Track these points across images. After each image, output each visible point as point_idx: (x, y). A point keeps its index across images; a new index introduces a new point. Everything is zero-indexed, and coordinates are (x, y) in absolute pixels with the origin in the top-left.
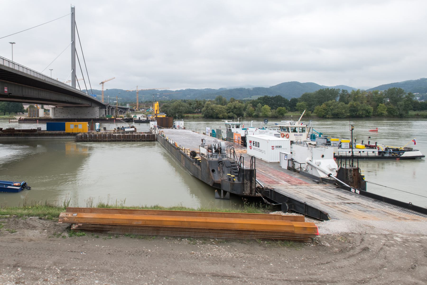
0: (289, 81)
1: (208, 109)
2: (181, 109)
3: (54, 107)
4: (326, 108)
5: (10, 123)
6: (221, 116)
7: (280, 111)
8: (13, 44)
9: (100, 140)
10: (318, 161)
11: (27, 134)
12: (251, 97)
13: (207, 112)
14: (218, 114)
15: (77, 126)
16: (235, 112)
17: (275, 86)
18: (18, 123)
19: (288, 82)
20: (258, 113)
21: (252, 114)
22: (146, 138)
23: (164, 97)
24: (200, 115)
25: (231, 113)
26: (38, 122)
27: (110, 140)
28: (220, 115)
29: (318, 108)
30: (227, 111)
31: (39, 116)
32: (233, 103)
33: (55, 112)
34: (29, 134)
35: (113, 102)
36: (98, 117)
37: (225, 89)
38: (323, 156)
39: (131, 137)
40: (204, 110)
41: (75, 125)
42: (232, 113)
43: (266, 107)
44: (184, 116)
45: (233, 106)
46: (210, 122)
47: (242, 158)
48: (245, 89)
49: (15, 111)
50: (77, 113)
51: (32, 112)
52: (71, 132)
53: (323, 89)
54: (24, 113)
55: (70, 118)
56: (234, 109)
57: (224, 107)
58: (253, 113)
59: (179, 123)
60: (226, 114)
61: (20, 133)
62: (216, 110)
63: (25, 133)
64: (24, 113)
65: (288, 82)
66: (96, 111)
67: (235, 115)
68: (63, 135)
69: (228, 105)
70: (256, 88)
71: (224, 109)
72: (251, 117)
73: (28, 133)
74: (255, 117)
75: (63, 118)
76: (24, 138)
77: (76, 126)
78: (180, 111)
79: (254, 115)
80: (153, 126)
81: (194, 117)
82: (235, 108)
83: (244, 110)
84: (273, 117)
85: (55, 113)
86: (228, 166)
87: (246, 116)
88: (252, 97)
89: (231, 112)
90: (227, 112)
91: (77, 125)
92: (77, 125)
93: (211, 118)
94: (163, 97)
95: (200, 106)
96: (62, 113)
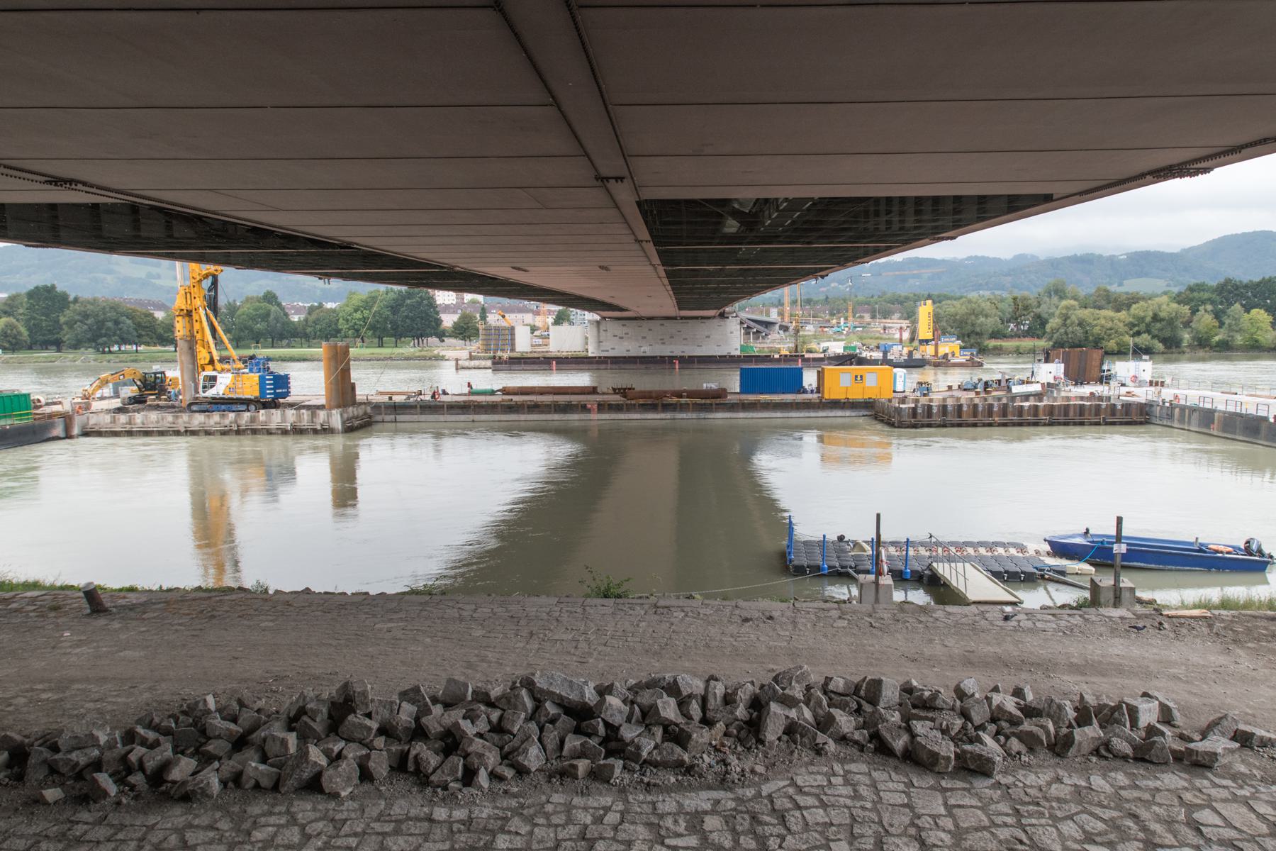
0: (1247, 231)
1: (1068, 321)
2: (981, 325)
3: (597, 317)
5: (461, 372)
11: (701, 405)
12: (1120, 285)
13: (1066, 333)
14: (1103, 339)
16: (1156, 332)
17: (1199, 247)
18: (490, 370)
19: (1244, 234)
20: (1232, 337)
21: (1208, 339)
22: (1118, 414)
23: (836, 284)
26: (554, 368)
27: (1003, 420)
28: (1110, 344)
31: (517, 350)
32: (1149, 302)
34: (711, 404)
36: (736, 349)
37: (1033, 256)
39: (1071, 413)
40: (1054, 325)
41: (856, 377)
44: (987, 346)
46: (731, 373)
48: (1100, 256)
49: (419, 332)
50: (672, 337)
51: (493, 337)
52: (841, 396)
54: (443, 341)
55: (648, 354)
56: (1153, 324)
57: (1122, 314)
61: (683, 400)
63: (699, 401)
64: (443, 341)
66: (731, 333)
67: (1156, 342)
68: (819, 408)
70: (1136, 253)
71: (1121, 325)
72: (1207, 349)
73: (708, 401)
75: (625, 354)
76: (694, 416)
77: (859, 378)
78: (978, 329)
79: (1217, 343)
81: (1021, 351)
82: (1156, 318)
83: (1187, 324)
85: (601, 339)
87: (1189, 346)
89: (1145, 332)
90: (1131, 332)
91: (861, 377)
92: (861, 377)
94: (832, 285)
95: (1025, 313)
96: (621, 338)
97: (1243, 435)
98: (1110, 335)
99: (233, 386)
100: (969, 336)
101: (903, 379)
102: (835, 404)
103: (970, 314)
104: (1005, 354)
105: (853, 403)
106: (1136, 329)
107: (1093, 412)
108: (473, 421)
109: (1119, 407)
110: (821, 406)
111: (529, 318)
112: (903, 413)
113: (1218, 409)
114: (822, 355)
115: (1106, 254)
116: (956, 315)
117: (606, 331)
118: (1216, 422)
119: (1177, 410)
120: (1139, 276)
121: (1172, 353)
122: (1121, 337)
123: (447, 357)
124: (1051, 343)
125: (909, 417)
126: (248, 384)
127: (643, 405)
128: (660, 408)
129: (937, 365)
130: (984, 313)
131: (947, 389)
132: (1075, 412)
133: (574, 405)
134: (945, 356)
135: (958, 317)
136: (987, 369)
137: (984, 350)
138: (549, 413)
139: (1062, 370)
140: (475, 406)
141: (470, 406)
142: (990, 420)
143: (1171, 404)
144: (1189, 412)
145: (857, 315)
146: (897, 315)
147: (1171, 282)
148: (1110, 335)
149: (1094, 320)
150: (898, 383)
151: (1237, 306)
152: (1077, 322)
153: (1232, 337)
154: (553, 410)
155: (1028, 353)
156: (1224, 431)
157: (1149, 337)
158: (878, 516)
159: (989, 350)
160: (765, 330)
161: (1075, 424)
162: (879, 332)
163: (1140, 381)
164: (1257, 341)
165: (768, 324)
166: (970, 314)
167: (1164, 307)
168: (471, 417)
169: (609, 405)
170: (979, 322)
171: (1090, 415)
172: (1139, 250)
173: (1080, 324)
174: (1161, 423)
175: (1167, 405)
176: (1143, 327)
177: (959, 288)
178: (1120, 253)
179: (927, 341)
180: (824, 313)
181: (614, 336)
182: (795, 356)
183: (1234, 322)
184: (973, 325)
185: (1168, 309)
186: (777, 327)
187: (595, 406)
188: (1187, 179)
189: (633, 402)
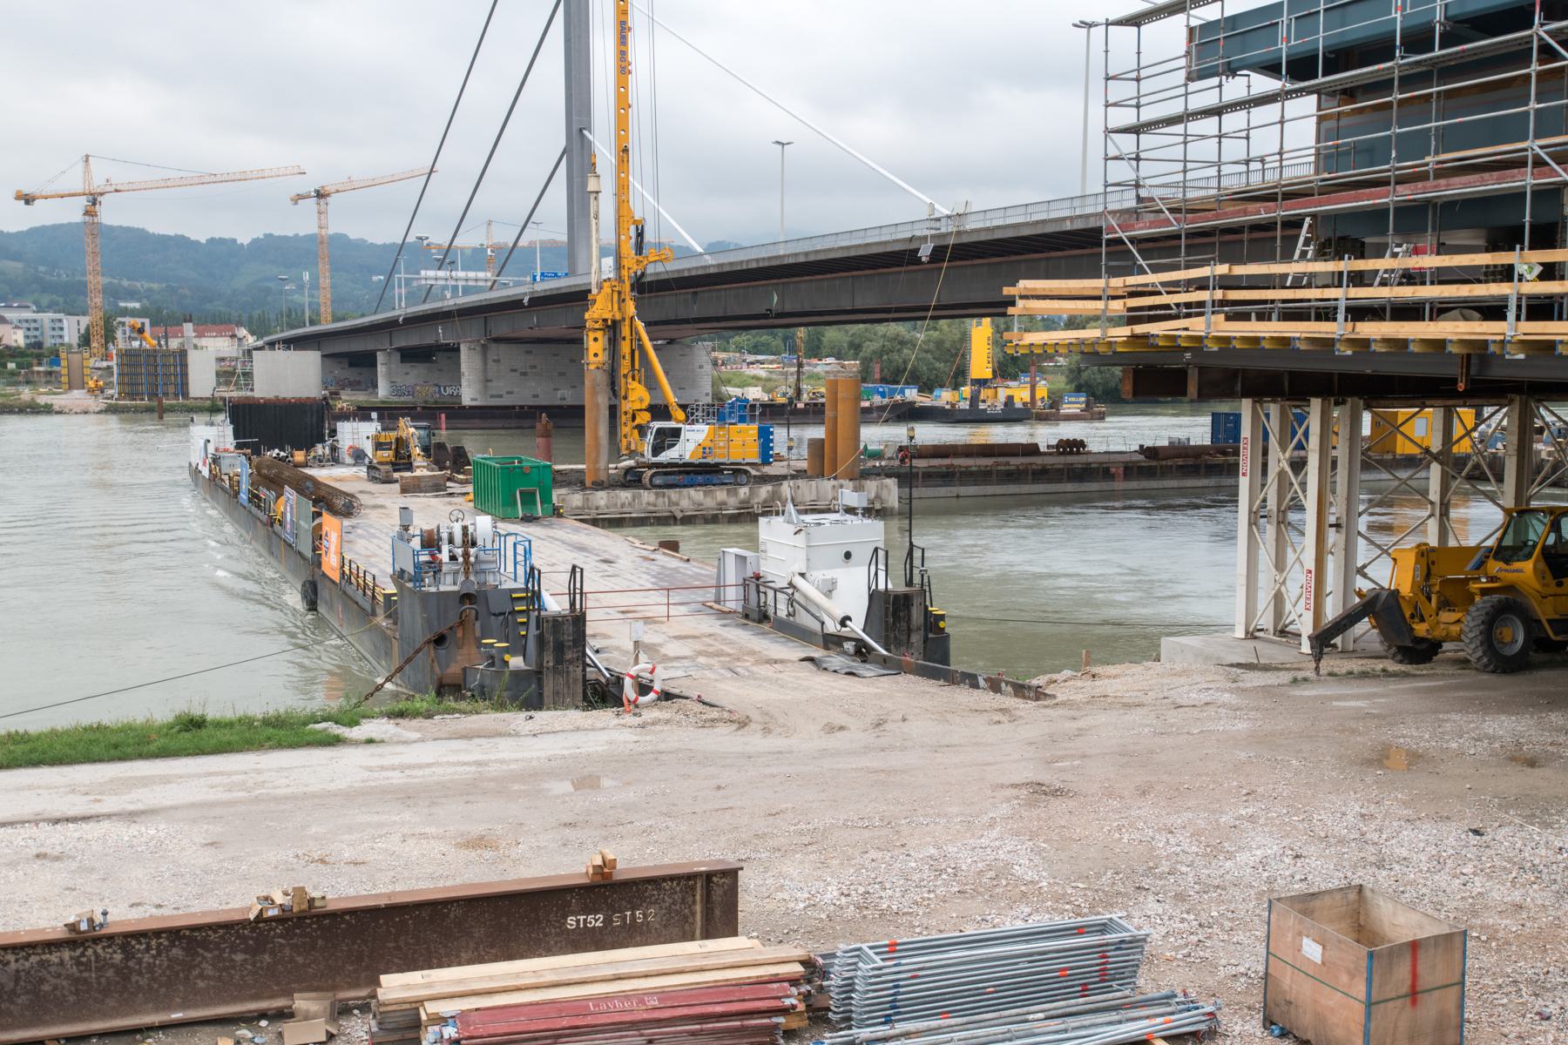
8: (1092, 29)
10: (830, 574)
26: (444, 426)
31: (191, 395)
33: (485, 370)
35: (117, 306)
38: (848, 555)
47: (578, 570)
66: (701, 367)
86: (497, 612)
96: (524, 374)
99: (711, 445)
108: (958, 497)
111: (446, 303)
117: (498, 361)
123: (56, 408)
126: (738, 440)
127: (1182, 466)
128: (1203, 470)
133: (1094, 469)
138: (1060, 481)
140: (961, 473)
141: (953, 474)
154: (1065, 477)
158: (796, 533)
168: (954, 490)
169: (1139, 467)
181: (513, 370)
187: (1121, 471)
188: (125, 225)
189: (1169, 463)
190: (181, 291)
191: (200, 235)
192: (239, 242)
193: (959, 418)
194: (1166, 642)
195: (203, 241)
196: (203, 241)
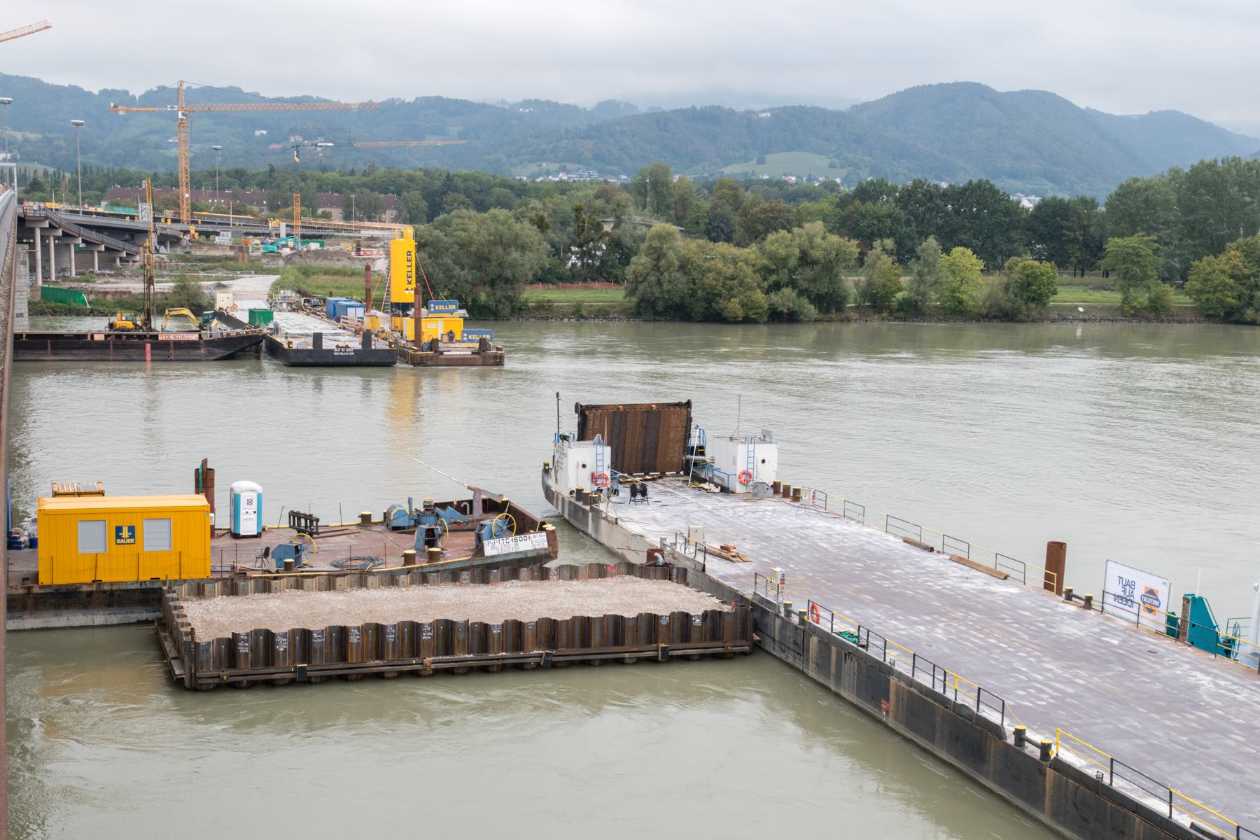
0: (945, 82)
1: (663, 262)
4: (1246, 272)
6: (734, 306)
7: (1029, 284)
9: (374, 664)
15: (132, 536)
16: (805, 285)
17: (877, 103)
20: (924, 294)
22: (695, 635)
24: (614, 295)
25: (787, 291)
29: (1209, 270)
30: (765, 279)
32: (796, 230)
39: (596, 637)
42: (794, 288)
43: (963, 256)
45: (797, 251)
48: (731, 112)
53: (1216, 161)
57: (751, 252)
58: (892, 293)
59: (750, 457)
60: (759, 296)
62: (709, 270)
65: (940, 85)
67: (805, 301)
69: (767, 245)
71: (749, 271)
72: (885, 314)
74: (901, 314)
77: (125, 533)
78: (508, 273)
80: (586, 474)
81: (584, 313)
84: (995, 317)
88: (768, 157)
90: (766, 284)
91: (132, 529)
92: (132, 529)
93: (672, 319)
97: (949, 752)
98: (731, 289)
100: (493, 284)
101: (254, 507)
102: (67, 598)
103: (495, 244)
104: (556, 318)
105: (112, 593)
106: (774, 278)
107: (643, 632)
109: (698, 622)
110: (30, 602)
112: (202, 657)
113: (897, 668)
114: (195, 337)
115: (740, 108)
116: (471, 244)
118: (892, 697)
119: (814, 640)
120: (790, 149)
121: (830, 321)
122: (749, 293)
124: (635, 300)
125: (218, 667)
129: (418, 362)
130: (519, 241)
131: (359, 521)
132: (603, 636)
134: (433, 344)
135: (473, 249)
136: (510, 372)
137: (520, 309)
139: (608, 461)
142: (414, 664)
143: (802, 622)
144: (838, 653)
145: (320, 211)
146: (390, 214)
147: (835, 160)
148: (731, 289)
149: (706, 260)
150: (243, 517)
151: (932, 242)
152: (677, 263)
153: (924, 294)
155: (596, 317)
156: (910, 725)
157: (794, 295)
159: (529, 309)
160: (127, 246)
161: (605, 663)
162: (347, 255)
163: (756, 485)
164: (961, 302)
165: (135, 235)
166: (495, 244)
167: (818, 240)
170: (509, 259)
171: (636, 640)
172: (790, 104)
173: (682, 267)
174: (783, 656)
175: (795, 619)
176: (783, 276)
177: (509, 157)
178: (761, 108)
179: (404, 307)
180: (259, 204)
182: (139, 337)
183: (926, 270)
184: (500, 265)
185: (824, 245)
186: (153, 238)
190: (56, 142)
191: (86, 89)
192: (130, 94)
193: (294, 360)
194: (1074, 599)
195: (96, 92)
196: (96, 92)
